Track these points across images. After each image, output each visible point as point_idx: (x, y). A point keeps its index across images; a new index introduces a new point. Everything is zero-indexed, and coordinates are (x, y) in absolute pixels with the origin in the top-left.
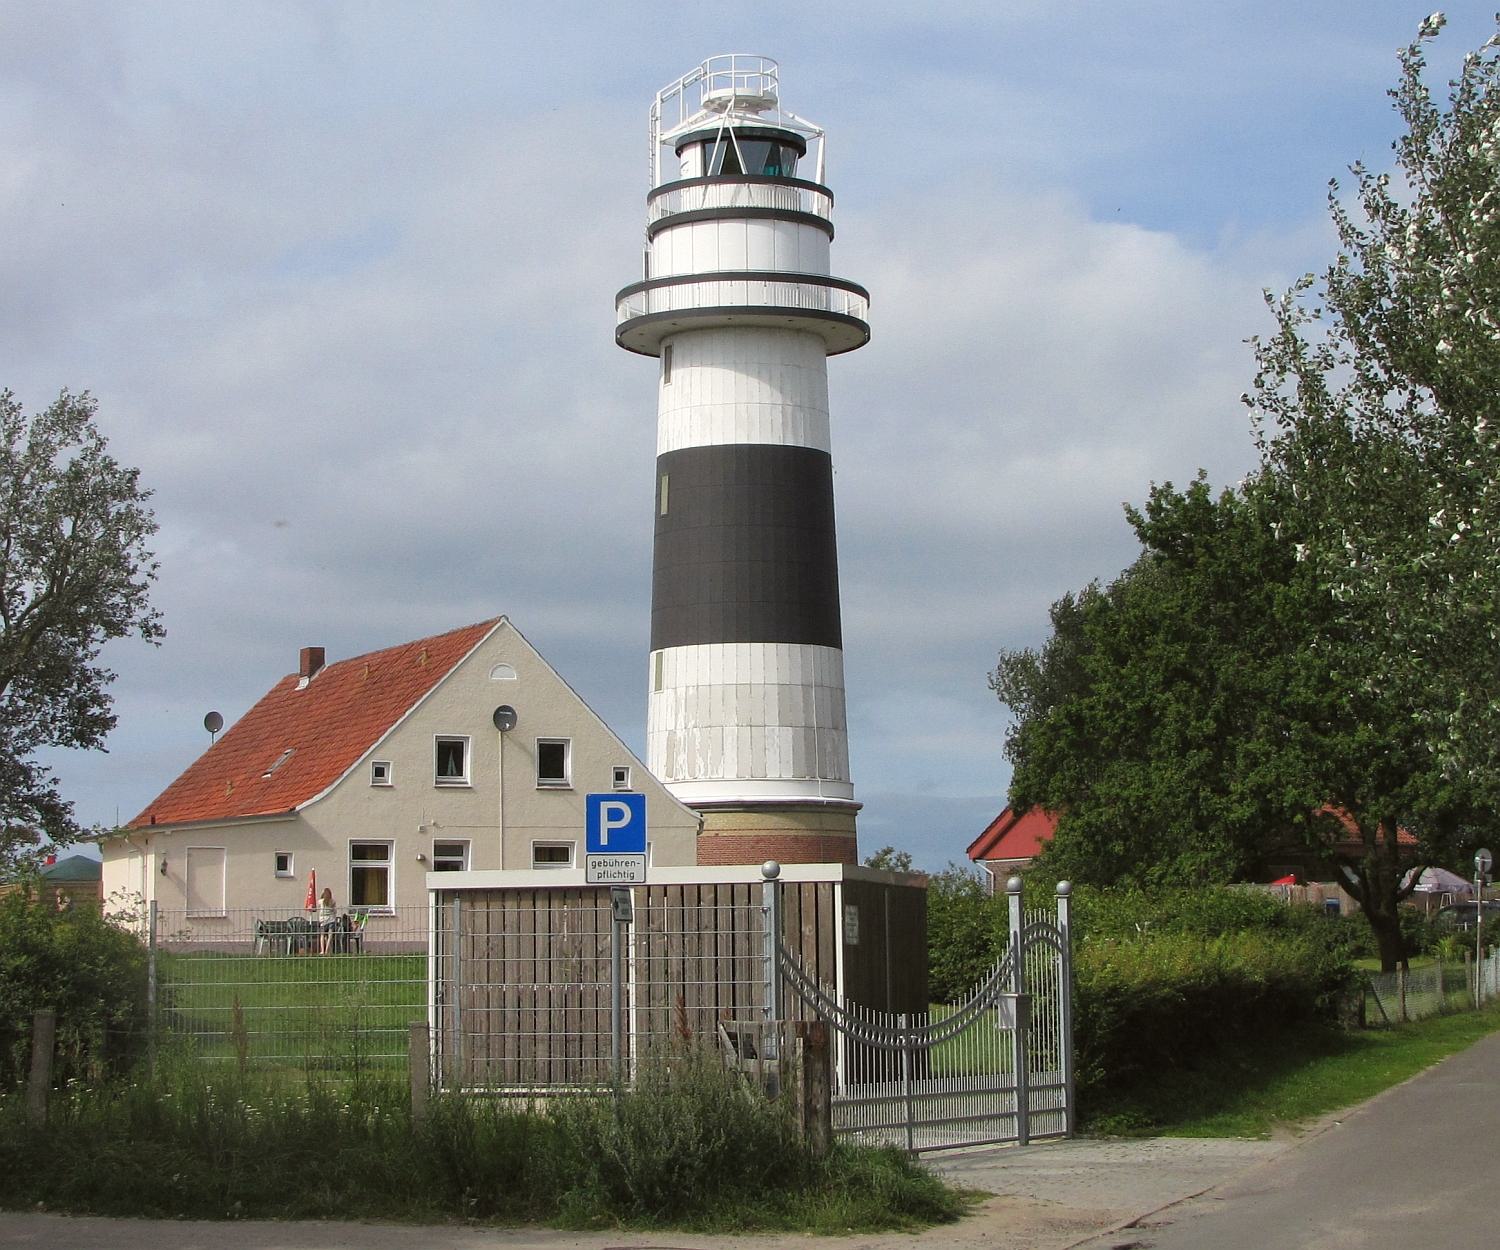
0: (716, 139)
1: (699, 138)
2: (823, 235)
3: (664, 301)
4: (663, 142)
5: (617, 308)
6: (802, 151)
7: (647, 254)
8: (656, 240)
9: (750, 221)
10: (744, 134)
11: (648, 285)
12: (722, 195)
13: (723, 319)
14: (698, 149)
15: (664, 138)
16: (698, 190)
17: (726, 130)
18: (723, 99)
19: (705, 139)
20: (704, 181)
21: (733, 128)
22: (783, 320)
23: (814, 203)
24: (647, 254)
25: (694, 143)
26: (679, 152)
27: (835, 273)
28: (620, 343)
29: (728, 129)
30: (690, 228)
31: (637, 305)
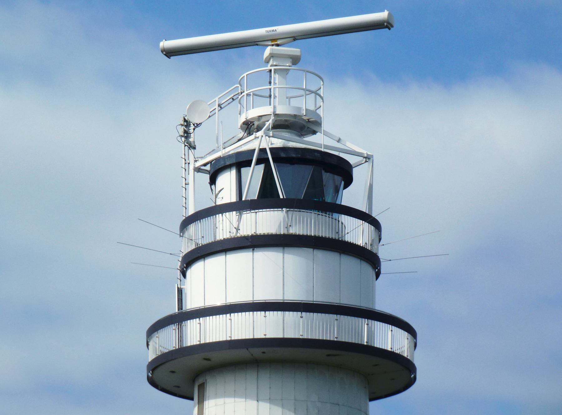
0: (252, 160)
1: (234, 161)
2: (371, 272)
3: (197, 333)
4: (198, 170)
5: (148, 345)
6: (348, 181)
7: (180, 291)
8: (189, 273)
9: (287, 249)
10: (282, 156)
11: (181, 317)
12: (268, 221)
13: (243, 354)
14: (234, 172)
15: (198, 164)
17: (263, 151)
19: (241, 162)
20: (241, 206)
21: (270, 149)
22: (320, 354)
23: (357, 233)
24: (180, 291)
26: (213, 181)
27: (380, 306)
28: (153, 382)
29: (265, 149)
31: (167, 340)
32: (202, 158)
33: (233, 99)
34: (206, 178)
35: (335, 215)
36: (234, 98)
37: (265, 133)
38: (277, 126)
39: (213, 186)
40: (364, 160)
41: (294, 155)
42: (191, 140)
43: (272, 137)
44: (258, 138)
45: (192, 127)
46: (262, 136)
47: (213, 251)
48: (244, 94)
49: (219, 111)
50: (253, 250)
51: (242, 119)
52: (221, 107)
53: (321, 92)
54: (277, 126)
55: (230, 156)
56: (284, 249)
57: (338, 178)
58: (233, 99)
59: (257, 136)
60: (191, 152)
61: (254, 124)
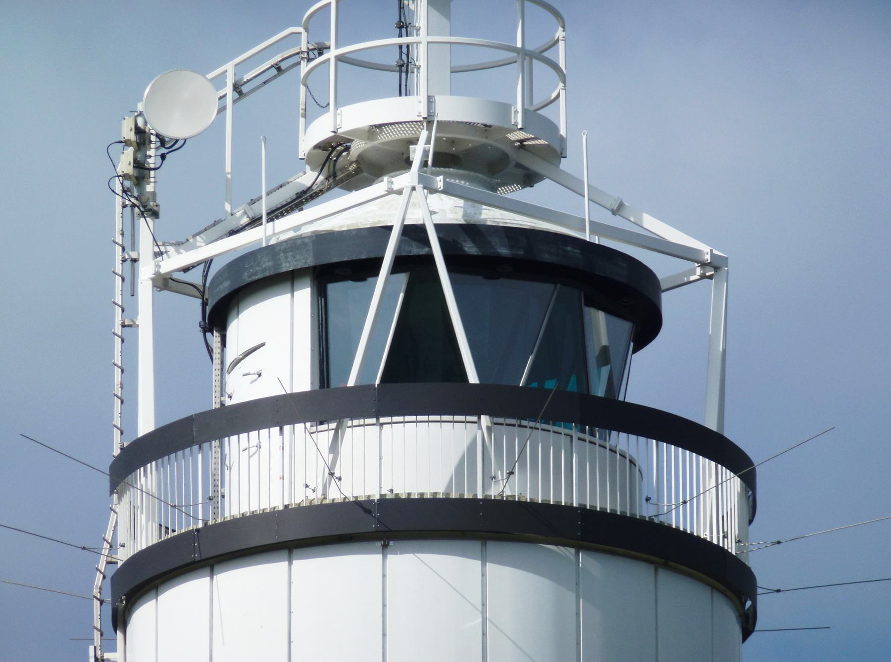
0: (379, 261)
1: (309, 261)
4: (164, 282)
6: (646, 324)
9: (492, 546)
10: (478, 254)
12: (415, 455)
14: (304, 295)
16: (305, 441)
17: (414, 233)
18: (386, 137)
19: (335, 268)
20: (327, 402)
21: (439, 227)
23: (701, 500)
25: (286, 279)
26: (217, 318)
30: (376, 559)
32: (178, 244)
33: (279, 69)
34: (192, 310)
35: (623, 441)
36: (283, 66)
37: (421, 179)
38: (445, 158)
39: (215, 339)
40: (699, 271)
41: (504, 251)
42: (149, 188)
43: (445, 192)
44: (400, 192)
45: (153, 153)
46: (414, 189)
47: (237, 547)
48: (331, 55)
49: (235, 101)
50: (385, 546)
51: (320, 130)
52: (240, 93)
53: (561, 56)
54: (445, 158)
55: (294, 245)
56: (484, 545)
57: (625, 327)
58: (279, 69)
59: (396, 187)
60: (145, 227)
61: (347, 149)
